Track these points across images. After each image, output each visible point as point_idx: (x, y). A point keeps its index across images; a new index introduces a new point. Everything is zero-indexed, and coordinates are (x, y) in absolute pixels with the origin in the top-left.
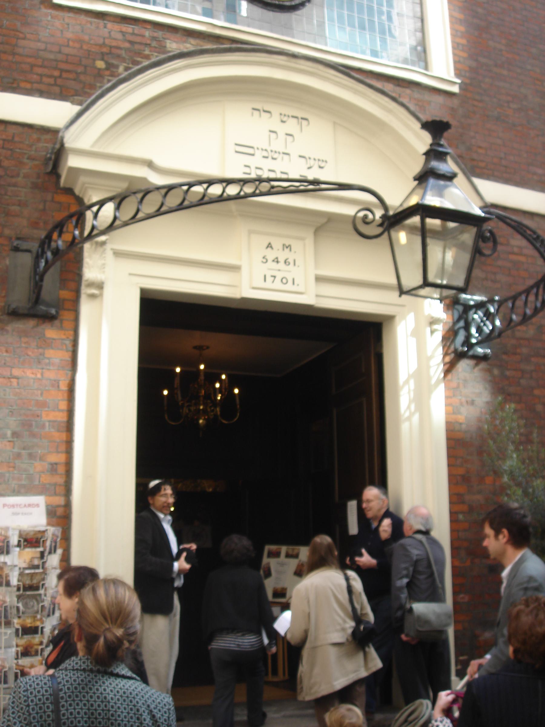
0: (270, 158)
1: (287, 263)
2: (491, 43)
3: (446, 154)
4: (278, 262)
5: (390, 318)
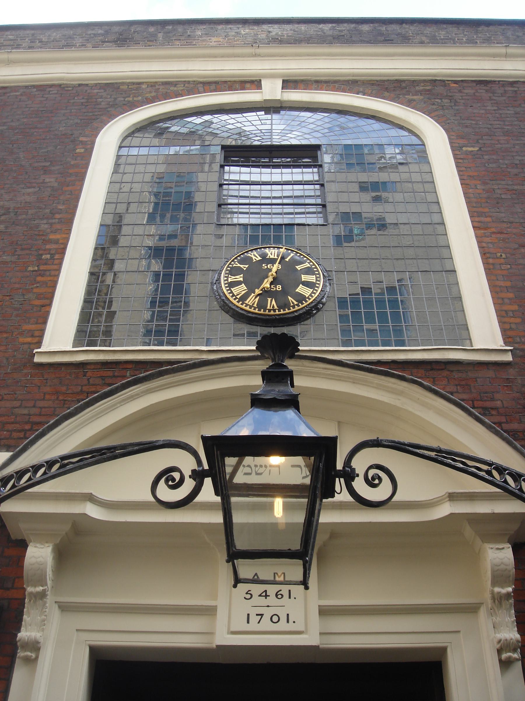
0: (254, 473)
1: (280, 596)
4: (266, 596)
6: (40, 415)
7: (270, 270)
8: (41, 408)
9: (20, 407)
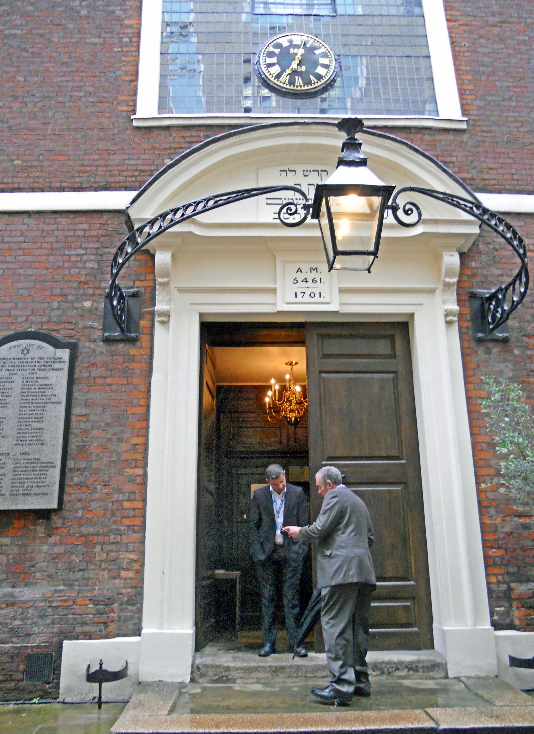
2: (498, 84)
3: (361, 144)
5: (412, 315)
6: (144, 165)
7: (296, 54)
8: (144, 160)
9: (129, 159)
